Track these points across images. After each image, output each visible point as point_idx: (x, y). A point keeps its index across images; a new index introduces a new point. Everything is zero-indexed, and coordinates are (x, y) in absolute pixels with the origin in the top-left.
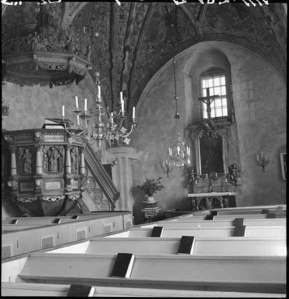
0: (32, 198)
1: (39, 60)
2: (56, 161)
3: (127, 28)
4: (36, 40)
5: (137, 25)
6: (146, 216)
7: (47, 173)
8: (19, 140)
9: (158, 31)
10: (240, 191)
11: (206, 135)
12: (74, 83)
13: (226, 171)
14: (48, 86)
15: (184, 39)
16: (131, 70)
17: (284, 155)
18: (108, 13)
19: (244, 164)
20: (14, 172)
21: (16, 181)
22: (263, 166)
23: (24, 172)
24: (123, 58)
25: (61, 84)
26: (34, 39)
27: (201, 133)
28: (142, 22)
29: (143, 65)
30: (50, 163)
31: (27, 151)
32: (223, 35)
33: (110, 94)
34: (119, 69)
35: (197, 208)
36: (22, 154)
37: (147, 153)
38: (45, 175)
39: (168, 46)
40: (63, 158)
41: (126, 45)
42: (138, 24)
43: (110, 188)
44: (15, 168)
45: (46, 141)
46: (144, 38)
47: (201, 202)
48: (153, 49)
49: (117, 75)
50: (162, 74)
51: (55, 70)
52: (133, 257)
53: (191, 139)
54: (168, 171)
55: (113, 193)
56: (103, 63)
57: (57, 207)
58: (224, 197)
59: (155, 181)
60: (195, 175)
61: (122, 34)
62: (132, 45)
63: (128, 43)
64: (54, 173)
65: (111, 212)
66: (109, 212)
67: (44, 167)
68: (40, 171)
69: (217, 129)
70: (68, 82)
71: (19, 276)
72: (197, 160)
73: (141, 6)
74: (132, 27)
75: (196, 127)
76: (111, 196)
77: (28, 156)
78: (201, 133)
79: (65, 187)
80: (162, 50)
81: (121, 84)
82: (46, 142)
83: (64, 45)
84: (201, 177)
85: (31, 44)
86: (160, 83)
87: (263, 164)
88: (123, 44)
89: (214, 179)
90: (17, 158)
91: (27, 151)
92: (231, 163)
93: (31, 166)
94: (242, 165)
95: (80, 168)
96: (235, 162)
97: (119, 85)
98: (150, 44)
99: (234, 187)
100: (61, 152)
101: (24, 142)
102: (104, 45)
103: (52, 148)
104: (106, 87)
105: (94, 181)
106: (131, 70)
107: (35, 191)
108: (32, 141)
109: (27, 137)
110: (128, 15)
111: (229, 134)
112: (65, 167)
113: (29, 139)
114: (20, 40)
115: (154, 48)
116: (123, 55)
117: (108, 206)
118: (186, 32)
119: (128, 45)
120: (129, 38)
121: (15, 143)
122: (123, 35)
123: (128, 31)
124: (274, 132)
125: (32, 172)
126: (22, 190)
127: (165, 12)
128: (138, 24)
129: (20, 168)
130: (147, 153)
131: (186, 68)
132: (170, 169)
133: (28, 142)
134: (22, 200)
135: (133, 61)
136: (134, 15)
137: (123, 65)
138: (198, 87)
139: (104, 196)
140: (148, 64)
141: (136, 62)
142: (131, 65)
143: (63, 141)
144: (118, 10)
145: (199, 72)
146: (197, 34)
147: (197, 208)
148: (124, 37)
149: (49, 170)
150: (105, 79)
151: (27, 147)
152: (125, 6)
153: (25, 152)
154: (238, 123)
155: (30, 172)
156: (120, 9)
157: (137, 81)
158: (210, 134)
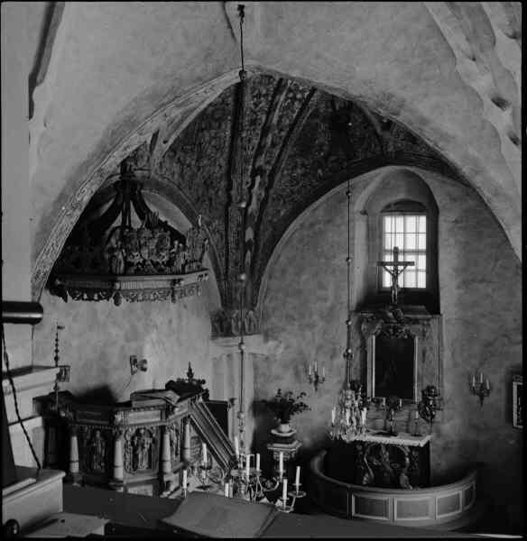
5: (279, 133)
7: (130, 473)
8: (85, 417)
9: (315, 140)
10: (439, 434)
11: (389, 332)
12: (112, 300)
13: (418, 398)
14: (112, 300)
15: (361, 156)
16: (263, 203)
17: (519, 386)
18: (229, 118)
19: (448, 388)
22: (482, 399)
24: (249, 185)
27: (378, 326)
30: (135, 456)
31: (98, 434)
32: (431, 159)
35: (365, 460)
37: (282, 346)
39: (330, 166)
41: (257, 165)
42: (281, 130)
46: (289, 150)
47: (371, 451)
48: (303, 169)
50: (315, 209)
53: (360, 333)
54: (316, 383)
56: (213, 197)
58: (411, 448)
59: (293, 397)
62: (268, 163)
63: (261, 162)
64: (141, 472)
69: (407, 323)
71: (34, 399)
72: (369, 371)
75: (371, 315)
76: (226, 460)
78: (378, 326)
80: (320, 171)
81: (245, 229)
83: (166, 259)
85: (111, 259)
86: (312, 225)
87: (482, 392)
88: (251, 163)
89: (395, 410)
91: (98, 434)
92: (426, 383)
94: (445, 389)
95: (183, 448)
96: (435, 383)
98: (299, 161)
99: (428, 426)
102: (218, 168)
110: (264, 119)
111: (427, 334)
112: (161, 461)
114: (91, 250)
115: (306, 168)
116: (250, 180)
118: (365, 146)
119: (261, 166)
120: (263, 156)
122: (253, 148)
123: (263, 143)
124: (506, 339)
125: (106, 470)
127: (330, 110)
130: (282, 346)
131: (359, 203)
132: (320, 378)
133: (100, 422)
135: (267, 190)
136: (275, 120)
137: (248, 196)
138: (378, 232)
139: (214, 461)
140: (292, 192)
141: (271, 192)
142: (263, 195)
143: (158, 419)
145: (383, 203)
146: (385, 152)
147: (365, 460)
148: (253, 153)
153: (93, 434)
154: (444, 316)
156: (252, 111)
158: (395, 329)
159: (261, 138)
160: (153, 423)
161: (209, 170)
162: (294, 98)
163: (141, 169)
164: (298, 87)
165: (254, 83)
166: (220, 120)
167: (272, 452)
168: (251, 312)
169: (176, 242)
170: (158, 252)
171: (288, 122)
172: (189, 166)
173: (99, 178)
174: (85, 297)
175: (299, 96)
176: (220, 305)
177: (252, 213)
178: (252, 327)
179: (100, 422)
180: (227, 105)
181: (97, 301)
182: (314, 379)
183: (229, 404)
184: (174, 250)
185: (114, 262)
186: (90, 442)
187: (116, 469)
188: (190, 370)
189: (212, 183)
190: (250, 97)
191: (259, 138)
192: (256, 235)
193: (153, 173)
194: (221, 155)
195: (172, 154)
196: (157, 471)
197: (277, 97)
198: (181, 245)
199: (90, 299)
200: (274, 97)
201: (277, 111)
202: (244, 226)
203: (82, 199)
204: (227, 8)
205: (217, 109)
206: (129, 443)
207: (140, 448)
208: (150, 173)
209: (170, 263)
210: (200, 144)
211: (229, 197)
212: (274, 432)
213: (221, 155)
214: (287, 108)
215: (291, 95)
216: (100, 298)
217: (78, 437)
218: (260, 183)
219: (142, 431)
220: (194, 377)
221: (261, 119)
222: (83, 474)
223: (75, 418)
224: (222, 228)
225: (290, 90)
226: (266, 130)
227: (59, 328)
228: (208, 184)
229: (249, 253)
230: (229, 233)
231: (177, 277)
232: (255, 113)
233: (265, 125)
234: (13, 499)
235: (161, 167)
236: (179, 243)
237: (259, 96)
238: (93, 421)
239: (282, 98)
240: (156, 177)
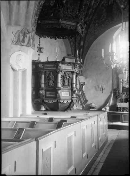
1: (62, 22)
2: (67, 80)
14: (54, 39)
20: (43, 85)
21: (44, 90)
23: (49, 86)
25: (62, 38)
36: (48, 75)
42: (93, 9)
44: (43, 83)
45: (63, 68)
51: (69, 29)
52: (25, 130)
57: (66, 106)
60: (119, 93)
65: (82, 110)
66: (81, 110)
68: (60, 85)
70: (66, 38)
76: (83, 101)
77: (52, 77)
79: (72, 95)
82: (63, 69)
84: (122, 94)
90: (45, 78)
93: (53, 83)
101: (50, 68)
103: (66, 72)
107: (56, 96)
108: (55, 68)
109: (53, 66)
112: (72, 84)
113: (54, 67)
117: (80, 107)
121: (45, 68)
126: (47, 96)
127: (107, 4)
128: (93, 9)
129: (47, 83)
132: (104, 89)
133: (53, 68)
134: (47, 101)
143: (72, 69)
149: (63, 85)
151: (52, 71)
153: (50, 74)
155: (53, 86)
159: (87, 12)
182: (102, 89)
186: (48, 77)
187: (58, 84)
196: (70, 88)
202: (80, 41)
204: (28, 114)
207: (65, 79)
217: (44, 75)
223: (44, 68)
226: (89, 9)
229: (81, 50)
230: (76, 42)
233: (89, 6)
234: (24, 98)
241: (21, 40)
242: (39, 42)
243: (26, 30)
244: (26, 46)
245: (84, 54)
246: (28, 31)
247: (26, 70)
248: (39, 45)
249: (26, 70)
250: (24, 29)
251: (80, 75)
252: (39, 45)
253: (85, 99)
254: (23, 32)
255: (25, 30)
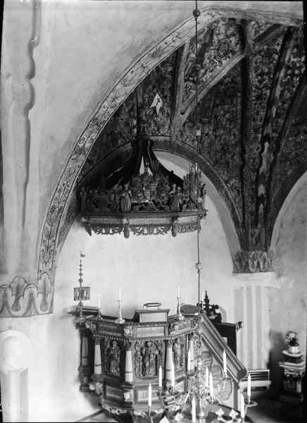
0: (120, 410)
3: (267, 111)
4: (127, 197)
5: (283, 105)
6: (285, 373)
14: (122, 233)
16: (272, 166)
24: (260, 150)
26: (124, 195)
28: (289, 102)
29: (290, 157)
31: (115, 344)
33: (240, 200)
34: (254, 166)
38: (140, 382)
40: (163, 357)
42: (284, 103)
43: (238, 364)
49: (252, 174)
55: (237, 368)
56: (230, 161)
61: (259, 119)
63: (268, 130)
67: (137, 370)
68: (130, 378)
73: (288, 79)
74: (274, 110)
81: (257, 186)
83: (166, 199)
91: (115, 344)
97: (254, 186)
100: (160, 348)
102: (233, 137)
104: (236, 192)
105: (210, 355)
106: (271, 166)
108: (119, 335)
110: (268, 94)
116: (260, 146)
120: (270, 125)
122: (261, 119)
123: (269, 115)
128: (284, 103)
129: (106, 365)
133: (115, 334)
135: (275, 154)
136: (278, 93)
142: (272, 158)
143: (163, 334)
144: (254, 89)
150: (234, 181)
152: (265, 82)
153: (111, 345)
157: (280, 180)
160: (159, 337)
161: (225, 139)
162: (293, 75)
163: (162, 135)
164: (295, 64)
165: (256, 63)
166: (233, 96)
167: (283, 369)
168: (265, 254)
169: (175, 186)
170: (158, 194)
171: (289, 95)
172: (207, 134)
173: (96, 127)
174: (104, 231)
175: (297, 72)
176: (239, 247)
177: (263, 173)
178: (266, 266)
179: (115, 334)
180: (236, 83)
181: (112, 234)
183: (237, 326)
184: (172, 192)
185: (123, 201)
187: (126, 374)
188: (206, 297)
189: (228, 149)
190: (254, 75)
191: (265, 110)
192: (267, 190)
193: (174, 139)
194: (235, 127)
195: (190, 124)
197: (278, 74)
198: (179, 188)
199: (107, 233)
200: (275, 75)
201: (279, 86)
202: (257, 182)
203: (84, 145)
205: (229, 88)
206: (139, 353)
207: (147, 358)
208: (171, 139)
209: (169, 203)
210: (216, 117)
211: (243, 160)
212: (285, 352)
213: (235, 127)
214: (288, 83)
215: (289, 72)
216: (114, 232)
218: (269, 148)
219: (149, 344)
220: (210, 303)
221: (265, 94)
222: (105, 376)
224: (238, 185)
225: (288, 68)
226: (271, 103)
227: (82, 256)
228: (225, 150)
231: (175, 214)
232: (260, 89)
235: (182, 135)
236: (177, 186)
237: (262, 74)
238: (111, 333)
239: (282, 74)
240: (178, 143)
241: (11, 306)
242: (81, 274)
243: (21, 280)
244: (24, 316)
245: (269, 215)
246: (26, 282)
247: (27, 370)
248: (81, 281)
249: (27, 370)
250: (17, 279)
251: (261, 271)
252: (81, 281)
253: (241, 368)
254: (15, 286)
255: (19, 280)
